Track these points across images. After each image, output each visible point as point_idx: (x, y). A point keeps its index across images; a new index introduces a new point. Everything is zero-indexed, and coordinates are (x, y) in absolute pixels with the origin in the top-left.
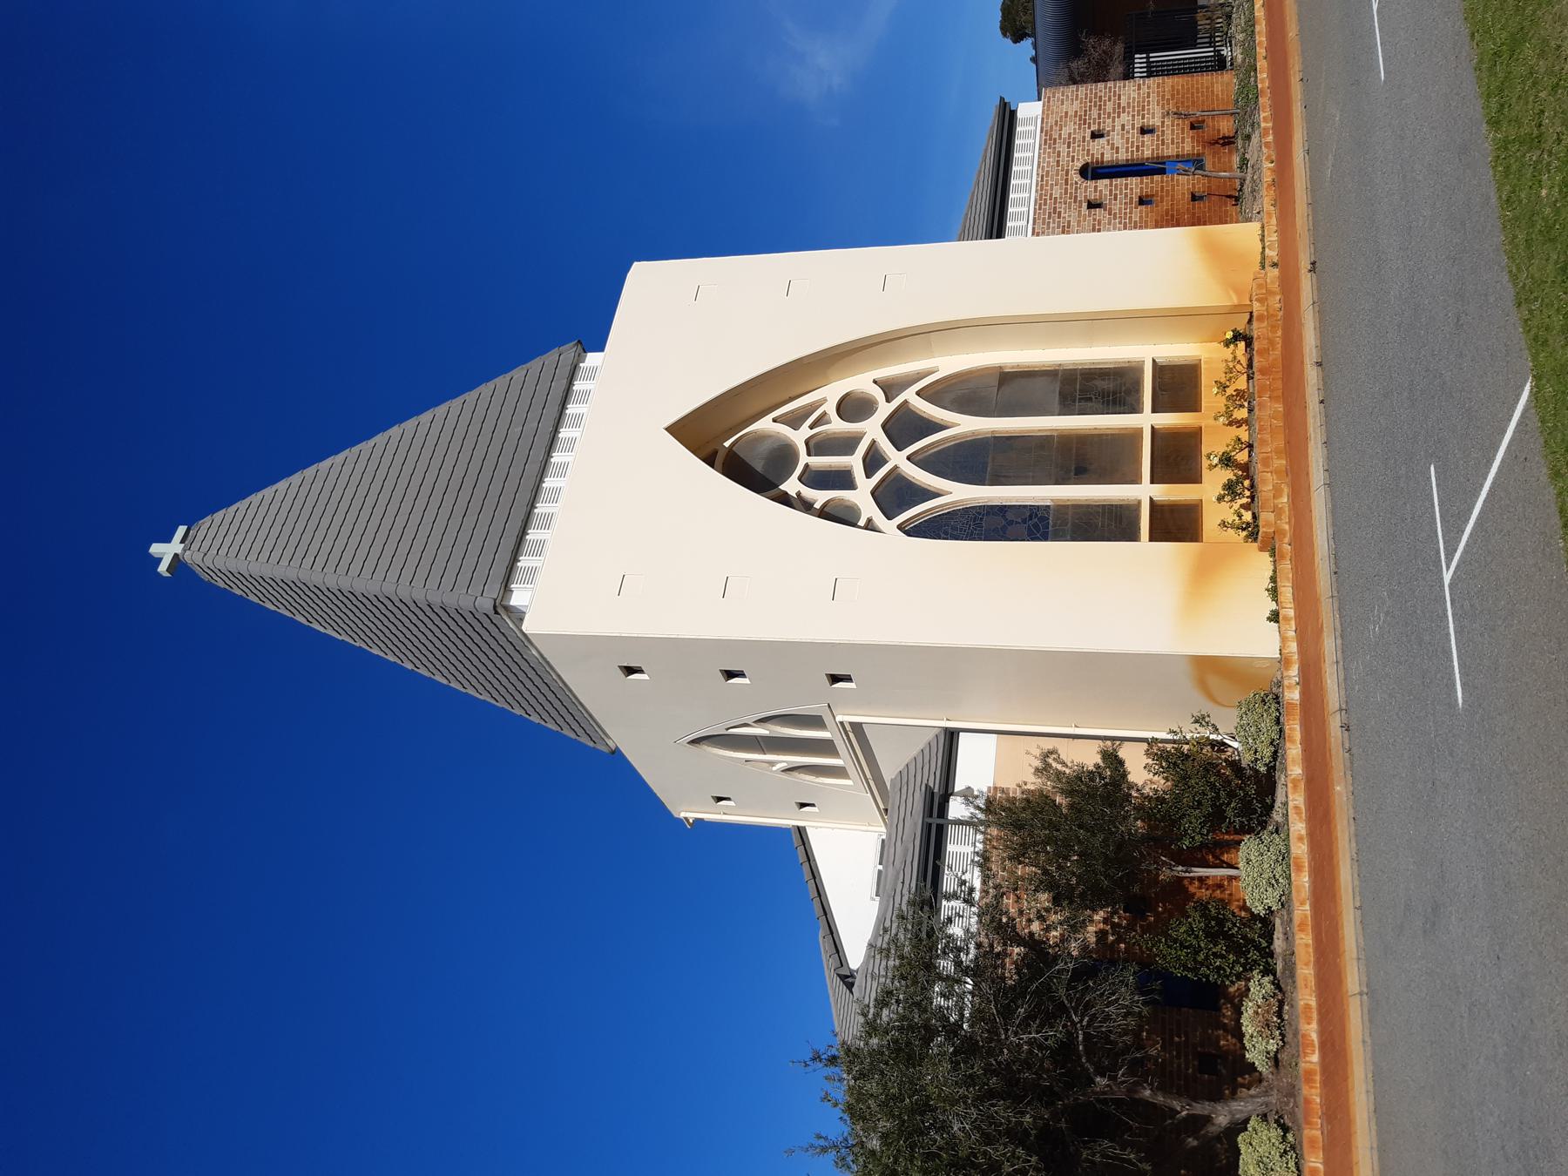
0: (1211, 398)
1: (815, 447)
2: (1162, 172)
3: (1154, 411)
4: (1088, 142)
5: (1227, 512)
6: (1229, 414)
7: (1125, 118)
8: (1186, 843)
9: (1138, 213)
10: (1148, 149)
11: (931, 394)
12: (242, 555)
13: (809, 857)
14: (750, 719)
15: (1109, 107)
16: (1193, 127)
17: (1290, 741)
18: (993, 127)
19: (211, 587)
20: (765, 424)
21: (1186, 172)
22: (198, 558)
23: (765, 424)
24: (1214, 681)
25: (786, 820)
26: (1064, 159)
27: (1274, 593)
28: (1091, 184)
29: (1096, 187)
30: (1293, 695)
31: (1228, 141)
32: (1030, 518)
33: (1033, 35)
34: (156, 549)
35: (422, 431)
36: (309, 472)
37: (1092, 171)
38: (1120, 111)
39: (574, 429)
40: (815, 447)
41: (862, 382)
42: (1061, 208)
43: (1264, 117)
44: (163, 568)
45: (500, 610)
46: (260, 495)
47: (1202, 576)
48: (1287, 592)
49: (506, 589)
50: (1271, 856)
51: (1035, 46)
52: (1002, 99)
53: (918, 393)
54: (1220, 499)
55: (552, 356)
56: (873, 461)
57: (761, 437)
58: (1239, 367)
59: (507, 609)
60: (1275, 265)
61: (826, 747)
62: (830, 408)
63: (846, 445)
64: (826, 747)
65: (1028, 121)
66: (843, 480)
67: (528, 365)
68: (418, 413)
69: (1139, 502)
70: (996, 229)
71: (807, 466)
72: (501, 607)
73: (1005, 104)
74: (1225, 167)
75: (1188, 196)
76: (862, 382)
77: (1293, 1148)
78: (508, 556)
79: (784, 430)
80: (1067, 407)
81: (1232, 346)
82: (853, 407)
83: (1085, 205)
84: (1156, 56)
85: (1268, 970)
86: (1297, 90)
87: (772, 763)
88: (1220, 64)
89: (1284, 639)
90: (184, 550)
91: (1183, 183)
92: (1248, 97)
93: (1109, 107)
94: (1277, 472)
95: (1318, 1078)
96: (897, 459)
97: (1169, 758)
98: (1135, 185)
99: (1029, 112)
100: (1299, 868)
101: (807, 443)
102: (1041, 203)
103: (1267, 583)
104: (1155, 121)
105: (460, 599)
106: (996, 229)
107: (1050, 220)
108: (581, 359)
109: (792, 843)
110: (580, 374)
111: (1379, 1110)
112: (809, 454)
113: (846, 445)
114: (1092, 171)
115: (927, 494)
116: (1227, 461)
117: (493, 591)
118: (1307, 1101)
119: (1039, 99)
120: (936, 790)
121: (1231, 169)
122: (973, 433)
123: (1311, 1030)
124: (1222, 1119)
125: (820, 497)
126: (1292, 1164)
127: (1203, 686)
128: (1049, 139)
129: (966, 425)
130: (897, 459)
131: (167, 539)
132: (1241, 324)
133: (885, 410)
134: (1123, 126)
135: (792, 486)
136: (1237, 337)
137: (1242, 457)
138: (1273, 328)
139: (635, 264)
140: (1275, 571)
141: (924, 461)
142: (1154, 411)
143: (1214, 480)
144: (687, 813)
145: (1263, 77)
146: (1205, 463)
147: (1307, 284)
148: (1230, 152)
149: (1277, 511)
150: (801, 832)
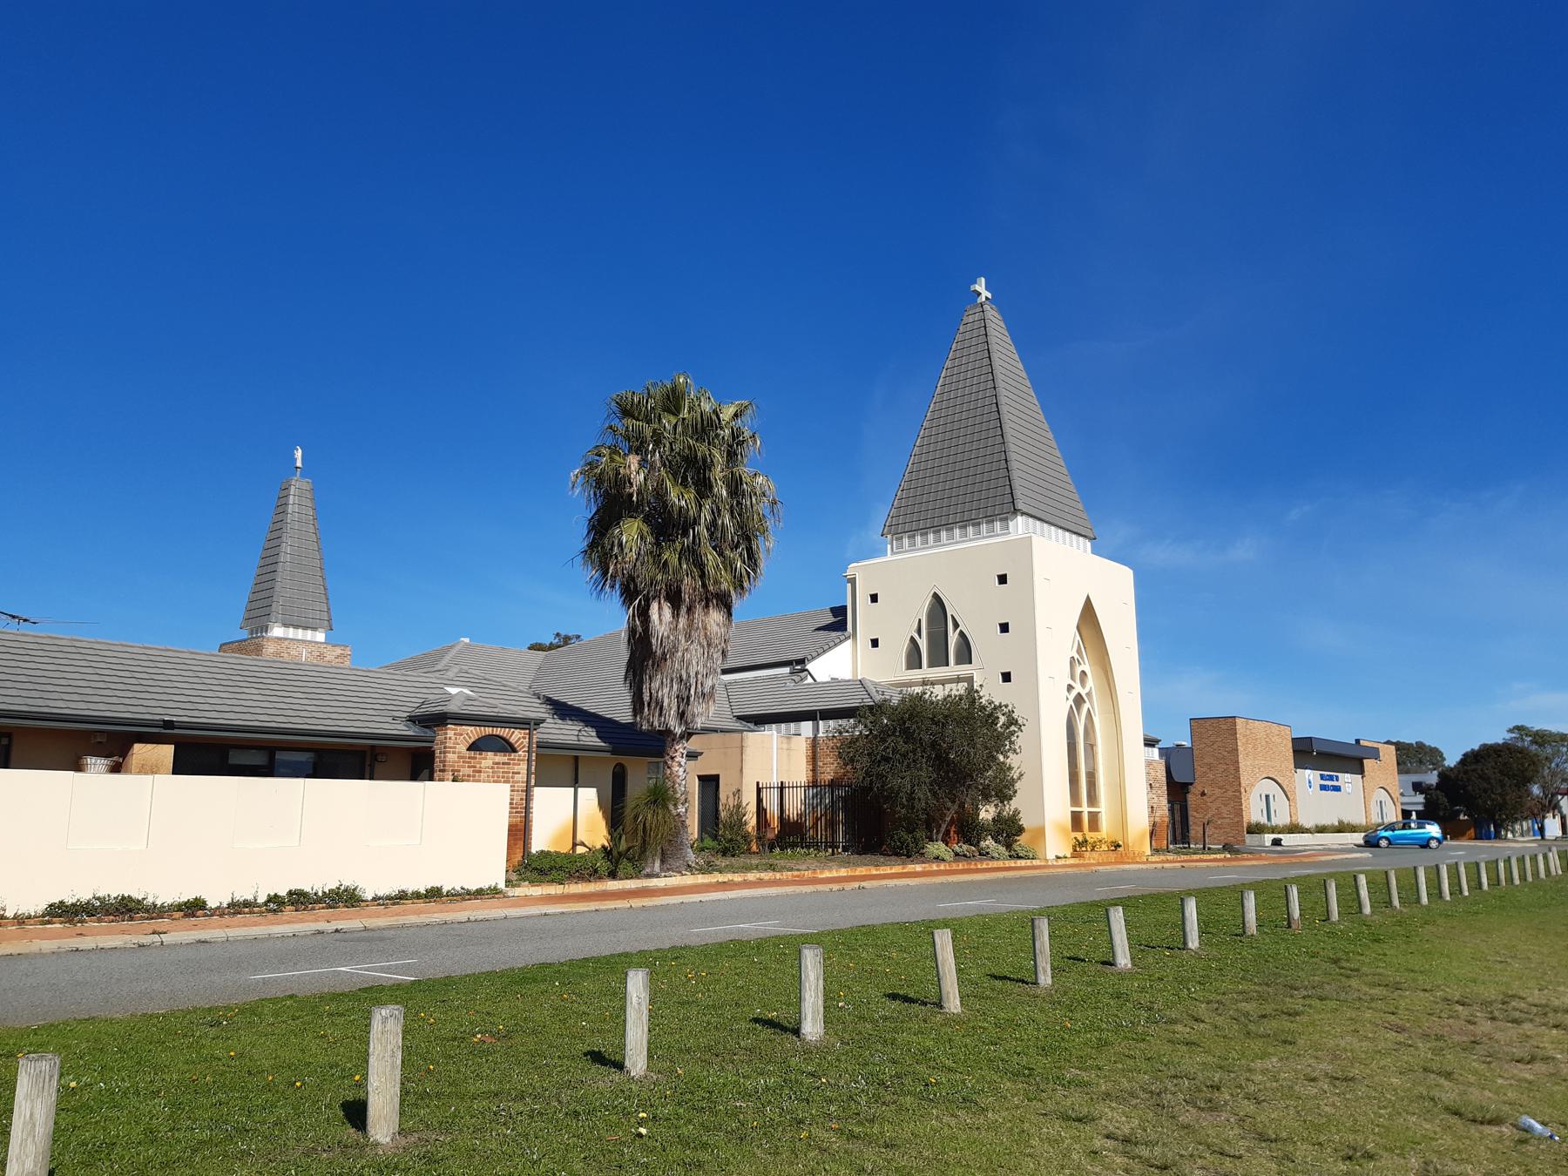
3: (1089, 812)
49: (1023, 514)
72: (1016, 511)
87: (919, 631)
142: (1089, 812)
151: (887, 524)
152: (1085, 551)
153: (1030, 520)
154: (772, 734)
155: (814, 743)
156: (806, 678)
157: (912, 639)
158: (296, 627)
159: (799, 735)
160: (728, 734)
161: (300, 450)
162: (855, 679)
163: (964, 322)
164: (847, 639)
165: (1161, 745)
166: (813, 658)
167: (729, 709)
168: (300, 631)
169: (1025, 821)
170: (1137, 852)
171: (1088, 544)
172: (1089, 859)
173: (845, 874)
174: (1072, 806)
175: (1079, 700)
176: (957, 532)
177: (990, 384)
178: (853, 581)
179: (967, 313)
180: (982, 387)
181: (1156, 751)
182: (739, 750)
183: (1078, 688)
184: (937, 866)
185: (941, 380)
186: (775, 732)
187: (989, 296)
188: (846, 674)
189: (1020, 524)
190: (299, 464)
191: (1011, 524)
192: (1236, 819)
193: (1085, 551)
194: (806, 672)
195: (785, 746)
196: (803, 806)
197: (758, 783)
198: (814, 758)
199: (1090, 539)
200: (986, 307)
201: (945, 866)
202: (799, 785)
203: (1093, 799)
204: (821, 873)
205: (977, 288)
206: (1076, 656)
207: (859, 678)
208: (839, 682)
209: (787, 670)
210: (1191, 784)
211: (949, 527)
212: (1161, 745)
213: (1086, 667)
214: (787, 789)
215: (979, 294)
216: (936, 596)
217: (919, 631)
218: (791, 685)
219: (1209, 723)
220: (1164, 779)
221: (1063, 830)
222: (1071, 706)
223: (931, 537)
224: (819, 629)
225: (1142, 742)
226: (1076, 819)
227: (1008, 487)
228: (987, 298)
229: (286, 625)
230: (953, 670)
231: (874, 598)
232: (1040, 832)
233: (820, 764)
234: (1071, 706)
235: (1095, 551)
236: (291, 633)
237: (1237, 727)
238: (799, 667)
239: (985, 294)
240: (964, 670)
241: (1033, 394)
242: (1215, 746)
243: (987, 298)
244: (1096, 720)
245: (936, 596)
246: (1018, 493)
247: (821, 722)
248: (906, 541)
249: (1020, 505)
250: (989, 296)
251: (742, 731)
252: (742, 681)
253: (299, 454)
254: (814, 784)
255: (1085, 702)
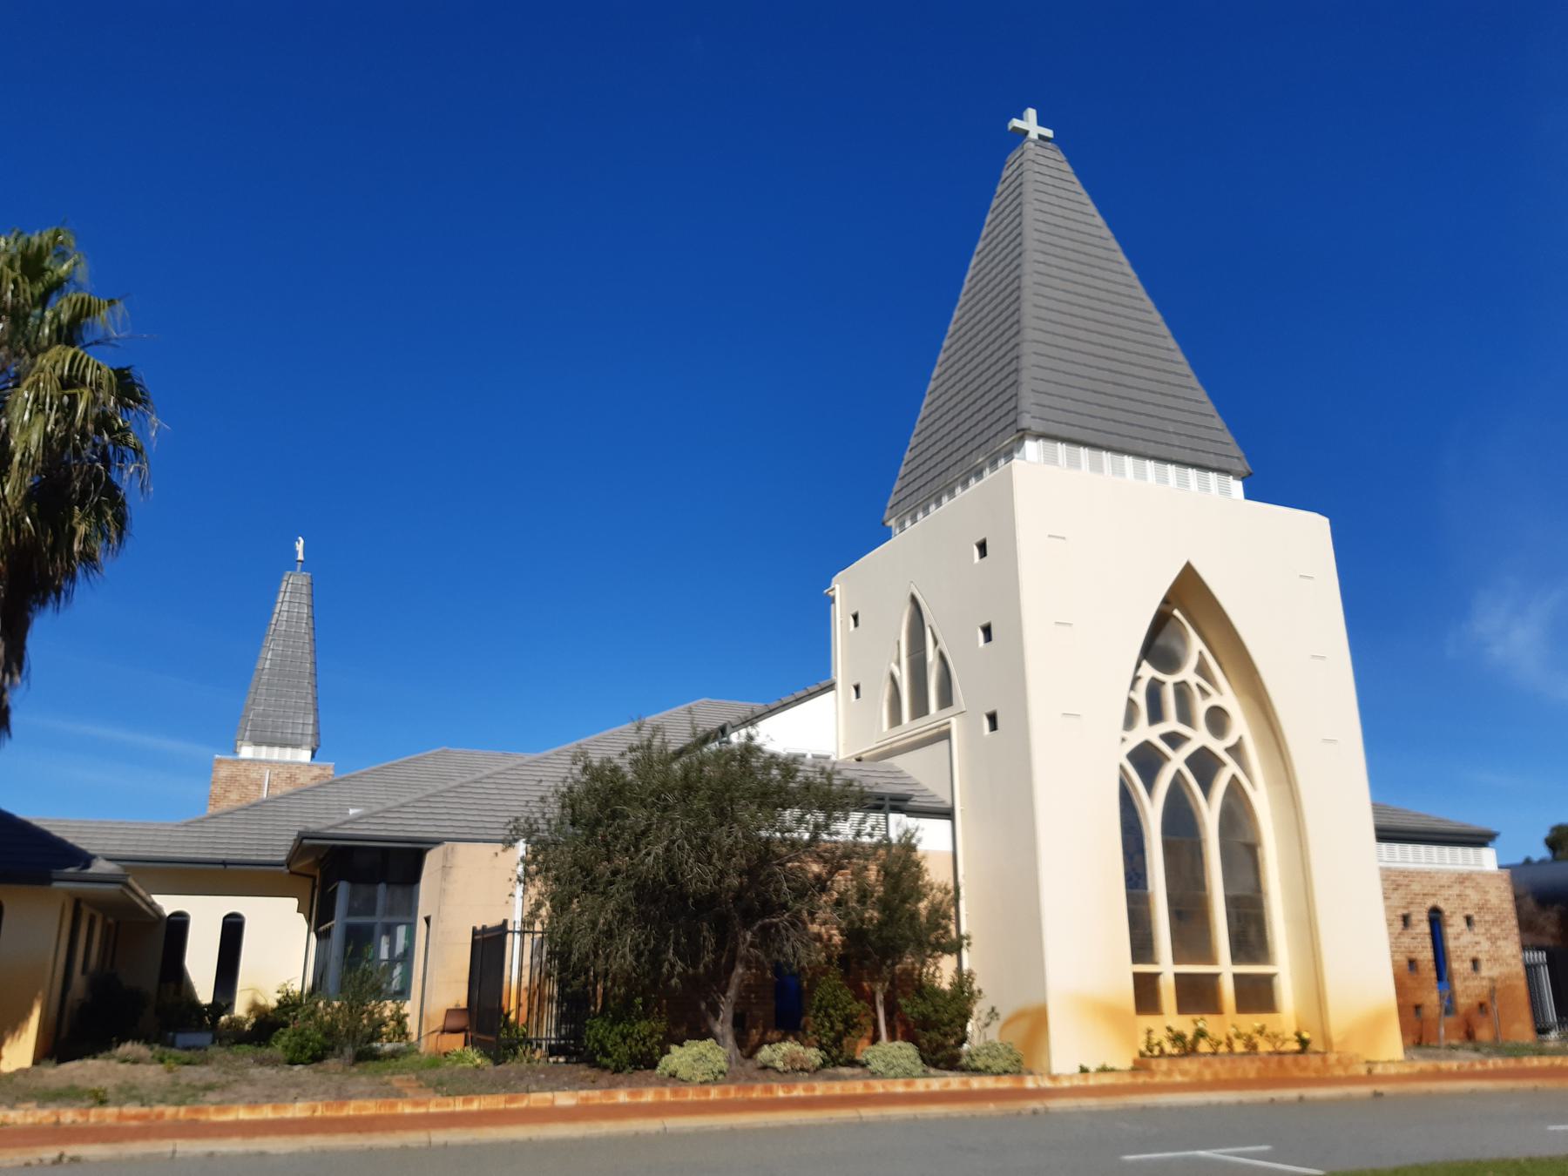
0: (1249, 1022)
1: (1182, 690)
2: (1440, 978)
3: (1238, 978)
5: (1160, 1035)
6: (1238, 1036)
7: (1485, 945)
8: (902, 1001)
9: (1403, 960)
10: (1459, 966)
11: (1234, 787)
12: (1038, 195)
13: (811, 695)
14: (943, 645)
15: (1495, 931)
16: (1481, 1005)
19: (1000, 164)
20: (1196, 644)
21: (1441, 997)
22: (1030, 155)
23: (1196, 644)
24: (1024, 1025)
25: (841, 672)
26: (1446, 893)
27: (1104, 1070)
28: (1424, 916)
29: (1422, 921)
30: (1030, 1083)
31: (1470, 1035)
32: (1137, 874)
33: (1555, 858)
34: (1031, 113)
35: (1158, 341)
36: (1114, 244)
37: (1436, 918)
38: (1493, 940)
40: (1182, 690)
41: (1241, 726)
42: (1402, 891)
44: (1016, 123)
45: (1020, 434)
46: (1088, 201)
47: (1109, 1013)
48: (1107, 1079)
49: (1038, 436)
50: (906, 1063)
51: (1542, 862)
53: (1234, 777)
54: (1169, 1029)
55: (1237, 452)
56: (1174, 740)
57: (1183, 639)
58: (1278, 1044)
59: (1021, 440)
60: (1370, 1071)
61: (920, 709)
62: (1215, 700)
63: (1185, 716)
64: (920, 709)
65: (1479, 859)
66: (1156, 715)
67: (1227, 431)
70: (1385, 835)
71: (1163, 683)
72: (1022, 435)
74: (1445, 1030)
75: (1418, 1002)
76: (1241, 726)
77: (716, 1079)
78: (1066, 435)
79: (1192, 662)
80: (1232, 902)
81: (1296, 1038)
82: (1218, 721)
83: (1405, 912)
84: (1544, 973)
85: (824, 1065)
86: (1528, 1084)
87: (898, 663)
88: (1542, 1030)
89: (1070, 1077)
90: (1034, 141)
91: (1431, 998)
92: (1517, 1051)
93: (1495, 931)
94: (1200, 1073)
96: (1177, 761)
97: (963, 986)
98: (1426, 955)
99: (1487, 860)
100: (908, 1085)
101: (1184, 682)
102: (1408, 875)
103: (1109, 1065)
104: (1485, 971)
105: (1027, 400)
106: (1385, 835)
107: (1394, 882)
108: (1237, 476)
109: (822, 680)
110: (1223, 477)
111: (791, 1129)
112: (1176, 684)
113: (1185, 716)
114: (1436, 918)
115: (1150, 785)
116: (1200, 1034)
117: (1037, 426)
118: (752, 1088)
119: (1500, 867)
120: (910, 803)
121: (1446, 1037)
122: (1204, 824)
123: (799, 1092)
124: (718, 1028)
125: (1141, 698)
126: (706, 1077)
127: (1019, 1016)
128: (1463, 879)
129: (1210, 815)
130: (1177, 761)
132: (1316, 1045)
133: (1218, 747)
134: (1477, 943)
135: (1148, 672)
136: (1304, 1043)
137: (1203, 1046)
138: (1317, 1071)
139: (1324, 522)
140: (1119, 1071)
141: (1177, 785)
143: (1185, 1025)
144: (840, 587)
145: (1535, 1062)
146: (1197, 1017)
147: (1364, 1090)
148: (1460, 1039)
149: (1169, 1073)
150: (831, 687)
158: (271, 744)
161: (302, 541)
168: (277, 750)
173: (307, 1114)
184: (675, 1093)
190: (301, 557)
229: (257, 743)
234: (1122, 767)
236: (264, 753)
253: (300, 546)
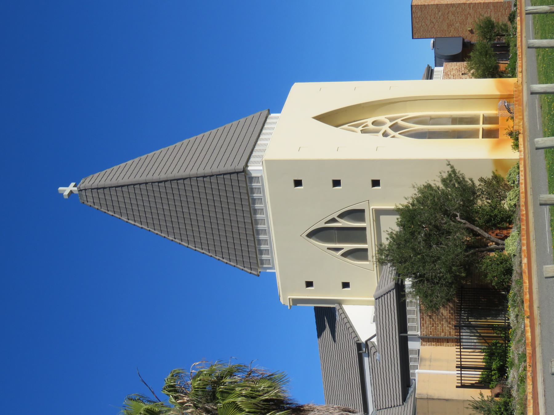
3: (483, 124)
4: (461, 76)
17: (525, 283)
18: (424, 75)
39: (258, 158)
43: (520, 56)
49: (246, 165)
52: (428, 65)
68: (197, 135)
69: (480, 115)
72: (244, 171)
73: (430, 67)
87: (337, 250)
95: (525, 215)
131: (67, 186)
142: (483, 124)
151: (249, 271)
152: (277, 118)
153: (252, 159)
154: (418, 373)
155: (426, 339)
156: (373, 343)
157: (345, 255)
159: (419, 350)
160: (417, 410)
162: (374, 303)
163: (92, 205)
164: (342, 308)
165: (432, 64)
166: (357, 336)
167: (397, 408)
169: (488, 175)
170: (515, 89)
171: (272, 115)
172: (519, 126)
174: (478, 138)
175: (395, 127)
176: (259, 216)
177: (143, 187)
178: (296, 302)
179: (86, 202)
180: (144, 192)
181: (436, 69)
182: (430, 402)
183: (386, 128)
185: (136, 224)
186: (416, 371)
187: (73, 184)
188: (369, 311)
189: (254, 168)
191: (254, 175)
192: (492, 8)
193: (277, 118)
194: (368, 342)
195: (428, 363)
196: (477, 350)
197: (457, 387)
198: (438, 340)
199: (269, 113)
200: (82, 185)
201: (523, 239)
202: (459, 357)
203: (473, 120)
204: (528, 339)
205: (66, 193)
206: (360, 128)
207: (374, 299)
208: (377, 316)
209: (366, 360)
210: (463, 40)
211: (254, 222)
212: (432, 64)
213: (369, 121)
214: (462, 363)
215: (71, 192)
216: (311, 235)
217: (337, 250)
218: (378, 356)
219: (416, 25)
220: (459, 63)
221: (498, 144)
222: (399, 134)
223: (262, 237)
224: (335, 341)
225: (429, 81)
226: (488, 134)
227: (225, 176)
228: (75, 186)
230: (368, 224)
231: (309, 284)
232: (498, 163)
233: (442, 335)
234: (399, 134)
235: (279, 111)
237: (419, 4)
238: (364, 349)
239: (71, 187)
240: (369, 216)
241: (153, 153)
242: (434, 21)
243: (75, 186)
244: (411, 114)
245: (311, 235)
246: (229, 168)
247: (409, 333)
248: (264, 257)
249: (240, 167)
250: (73, 184)
251: (415, 399)
252: (374, 395)
254: (458, 341)
255: (397, 123)
